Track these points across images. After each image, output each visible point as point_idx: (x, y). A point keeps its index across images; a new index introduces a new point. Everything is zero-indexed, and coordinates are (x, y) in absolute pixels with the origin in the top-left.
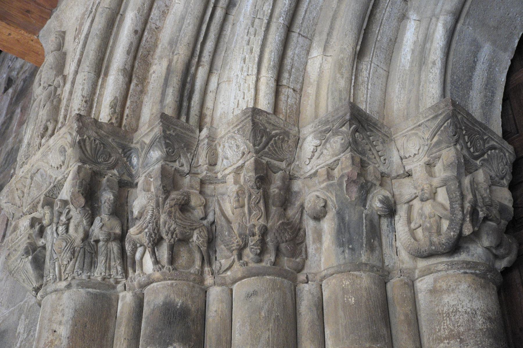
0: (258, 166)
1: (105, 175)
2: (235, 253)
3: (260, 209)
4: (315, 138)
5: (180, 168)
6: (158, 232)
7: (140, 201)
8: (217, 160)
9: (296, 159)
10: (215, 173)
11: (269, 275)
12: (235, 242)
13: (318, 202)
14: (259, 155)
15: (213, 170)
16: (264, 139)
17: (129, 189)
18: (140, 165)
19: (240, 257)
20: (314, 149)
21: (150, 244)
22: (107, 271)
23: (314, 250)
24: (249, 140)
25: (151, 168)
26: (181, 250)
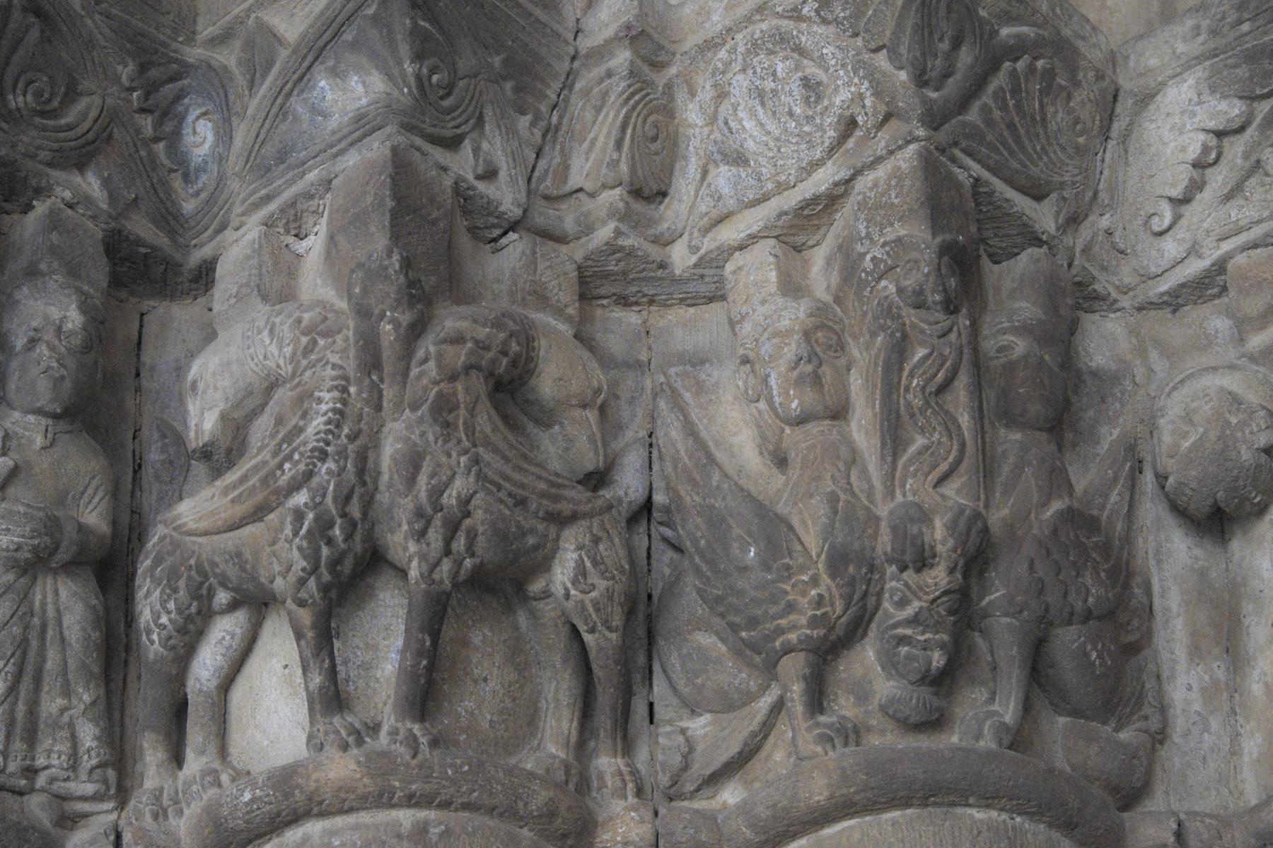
0: (940, 198)
1: (39, 192)
2: (793, 667)
3: (950, 426)
4: (1213, 89)
5: (481, 187)
6: (365, 515)
7: (231, 360)
8: (668, 171)
9: (1104, 196)
10: (656, 241)
11: (988, 800)
12: (803, 602)
13: (1244, 423)
14: (942, 136)
15: (651, 222)
16: (966, 57)
17: (147, 304)
18: (234, 162)
19: (817, 699)
20: (1206, 149)
21: (312, 583)
22: (18, 745)
23: (1195, 695)
24: (892, 50)
25: (312, 176)
26: (476, 639)
